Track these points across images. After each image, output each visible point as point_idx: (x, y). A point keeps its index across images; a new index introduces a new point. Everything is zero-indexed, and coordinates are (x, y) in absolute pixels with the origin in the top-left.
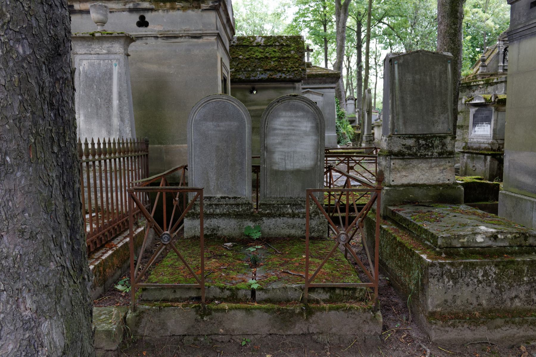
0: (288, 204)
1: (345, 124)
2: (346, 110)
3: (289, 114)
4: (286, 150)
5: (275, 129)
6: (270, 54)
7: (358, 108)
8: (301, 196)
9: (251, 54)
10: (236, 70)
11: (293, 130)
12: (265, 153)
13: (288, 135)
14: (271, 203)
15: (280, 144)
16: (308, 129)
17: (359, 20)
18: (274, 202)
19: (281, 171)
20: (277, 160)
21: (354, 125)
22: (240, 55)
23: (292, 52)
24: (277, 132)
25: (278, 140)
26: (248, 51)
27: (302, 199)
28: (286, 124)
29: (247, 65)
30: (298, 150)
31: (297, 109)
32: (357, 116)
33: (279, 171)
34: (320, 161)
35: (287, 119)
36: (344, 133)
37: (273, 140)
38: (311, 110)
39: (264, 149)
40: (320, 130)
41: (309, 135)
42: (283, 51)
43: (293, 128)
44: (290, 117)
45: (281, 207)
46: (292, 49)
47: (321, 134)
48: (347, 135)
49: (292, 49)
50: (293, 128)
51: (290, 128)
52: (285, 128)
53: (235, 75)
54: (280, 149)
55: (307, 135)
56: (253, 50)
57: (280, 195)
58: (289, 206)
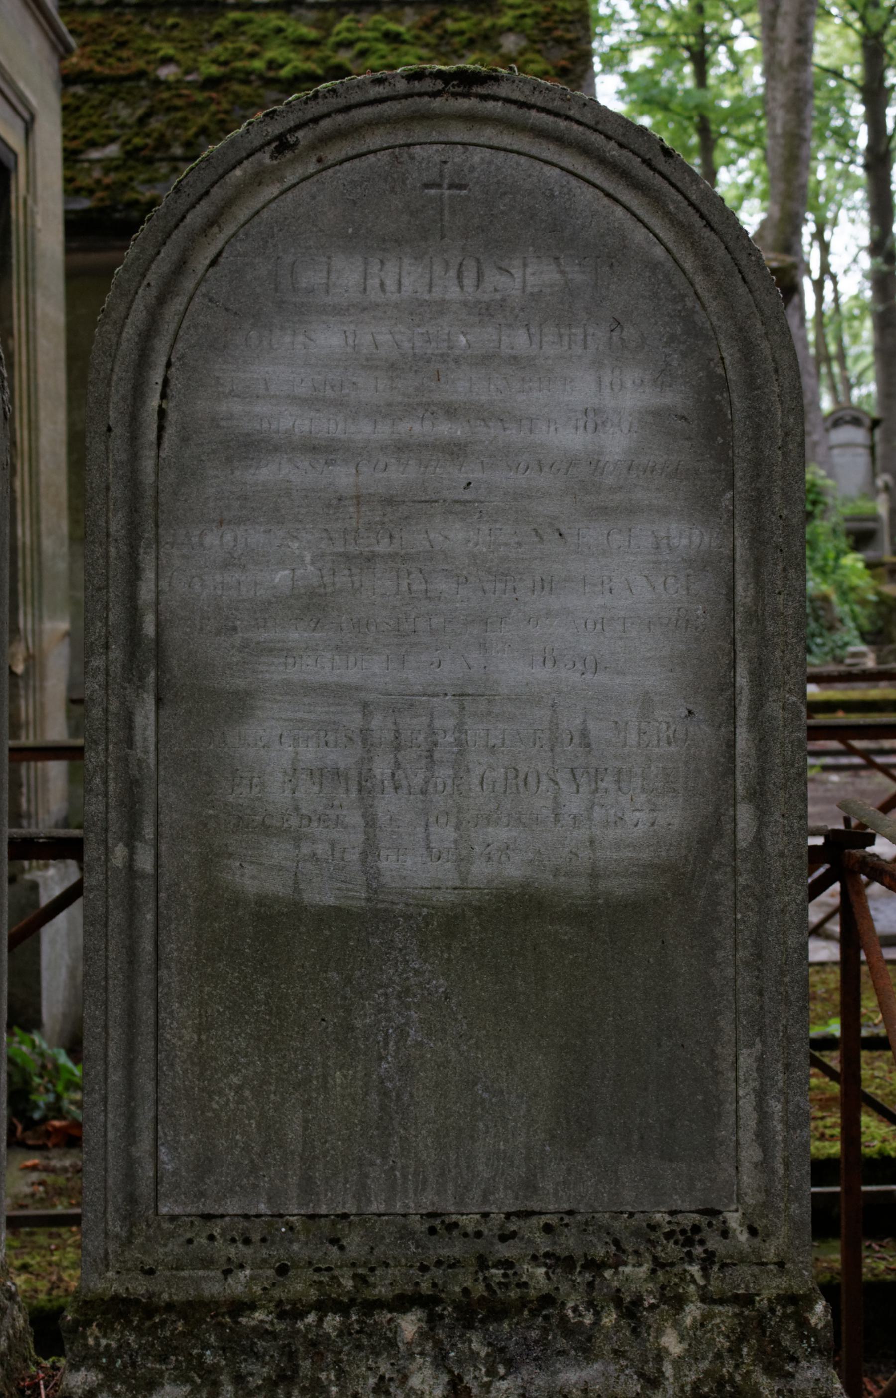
0: (402, 1303)
1: (828, 546)
2: (830, 475)
3: (403, 277)
4: (374, 671)
5: (251, 446)
6: (363, 54)
7: (885, 470)
8: (551, 1200)
9: (238, 53)
10: (132, 154)
11: (456, 451)
12: (145, 716)
13: (397, 507)
14: (213, 1288)
15: (312, 605)
16: (616, 443)
17: (875, 26)
18: (239, 1284)
19: (325, 916)
20: (278, 794)
21: (871, 554)
22: (166, 60)
23: (510, 43)
24: (268, 473)
25: (285, 562)
26: (219, 37)
27: (569, 1242)
28: (372, 388)
29: (203, 120)
30: (513, 672)
31: (487, 226)
32: (881, 506)
33: (296, 910)
34: (758, 795)
35: (383, 336)
36: (825, 599)
37: (228, 568)
38: (648, 237)
39: (133, 668)
40: (742, 449)
41: (632, 511)
42: (446, 35)
43: (445, 429)
44: (420, 310)
45: (316, 1346)
46: (506, 19)
47: (758, 500)
48: (841, 609)
49: (506, 19)
50: (445, 429)
51: (415, 428)
52: (365, 431)
53: (124, 185)
54: (313, 660)
55: (603, 511)
56: (250, 29)
57: (307, 1187)
58: (409, 1325)
